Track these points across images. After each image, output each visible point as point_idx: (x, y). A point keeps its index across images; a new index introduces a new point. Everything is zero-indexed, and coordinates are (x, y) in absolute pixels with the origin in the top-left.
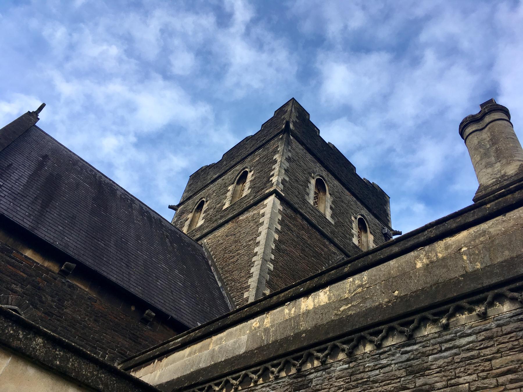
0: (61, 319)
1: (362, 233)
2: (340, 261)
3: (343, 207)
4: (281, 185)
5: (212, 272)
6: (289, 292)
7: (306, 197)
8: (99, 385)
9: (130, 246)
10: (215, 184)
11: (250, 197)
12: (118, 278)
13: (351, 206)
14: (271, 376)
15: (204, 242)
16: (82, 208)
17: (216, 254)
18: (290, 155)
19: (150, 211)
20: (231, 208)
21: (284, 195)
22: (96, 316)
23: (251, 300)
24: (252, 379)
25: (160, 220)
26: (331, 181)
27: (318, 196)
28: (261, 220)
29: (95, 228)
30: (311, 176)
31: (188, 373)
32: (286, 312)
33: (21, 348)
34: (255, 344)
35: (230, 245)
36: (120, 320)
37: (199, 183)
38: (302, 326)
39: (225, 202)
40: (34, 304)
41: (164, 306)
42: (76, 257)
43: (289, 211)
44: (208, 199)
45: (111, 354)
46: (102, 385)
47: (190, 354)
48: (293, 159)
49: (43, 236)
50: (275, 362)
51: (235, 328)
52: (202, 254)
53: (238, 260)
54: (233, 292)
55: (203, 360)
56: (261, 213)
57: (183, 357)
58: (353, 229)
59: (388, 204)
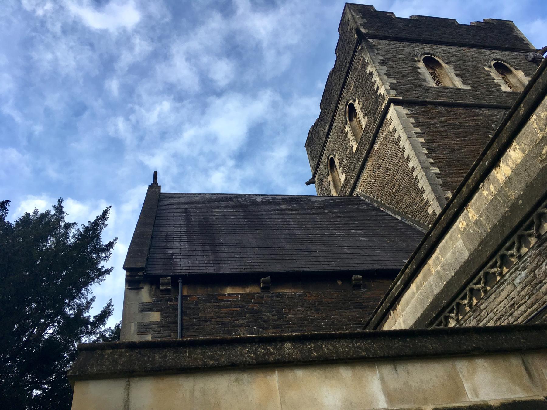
0: (290, 325)
1: (507, 76)
2: (503, 118)
3: (469, 66)
5: (384, 212)
6: (475, 174)
7: (425, 84)
8: (361, 353)
9: (300, 236)
10: (331, 137)
11: (370, 124)
12: (309, 266)
13: (477, 59)
14: (513, 259)
15: (358, 192)
16: (241, 231)
17: (376, 194)
19: (294, 198)
20: (360, 146)
21: (401, 98)
22: (315, 306)
23: (438, 211)
24: (494, 273)
25: (307, 199)
26: (439, 51)
27: (435, 74)
28: (396, 136)
29: (263, 240)
30: (416, 61)
31: (428, 304)
32: (485, 195)
33: (278, 359)
34: (475, 242)
35: (383, 178)
36: (335, 298)
37: (317, 146)
38: (512, 196)
39: (351, 145)
40: (262, 326)
41: (364, 265)
42: (265, 270)
43: (417, 109)
44: (334, 153)
45: (349, 329)
46: (364, 352)
47: (418, 289)
48: (386, 59)
49: (229, 270)
50: (508, 244)
51: (444, 241)
52: (364, 203)
53: (400, 185)
54: (415, 216)
55: (433, 287)
56: (391, 130)
57: (414, 295)
58: (495, 80)
59: (515, 29)
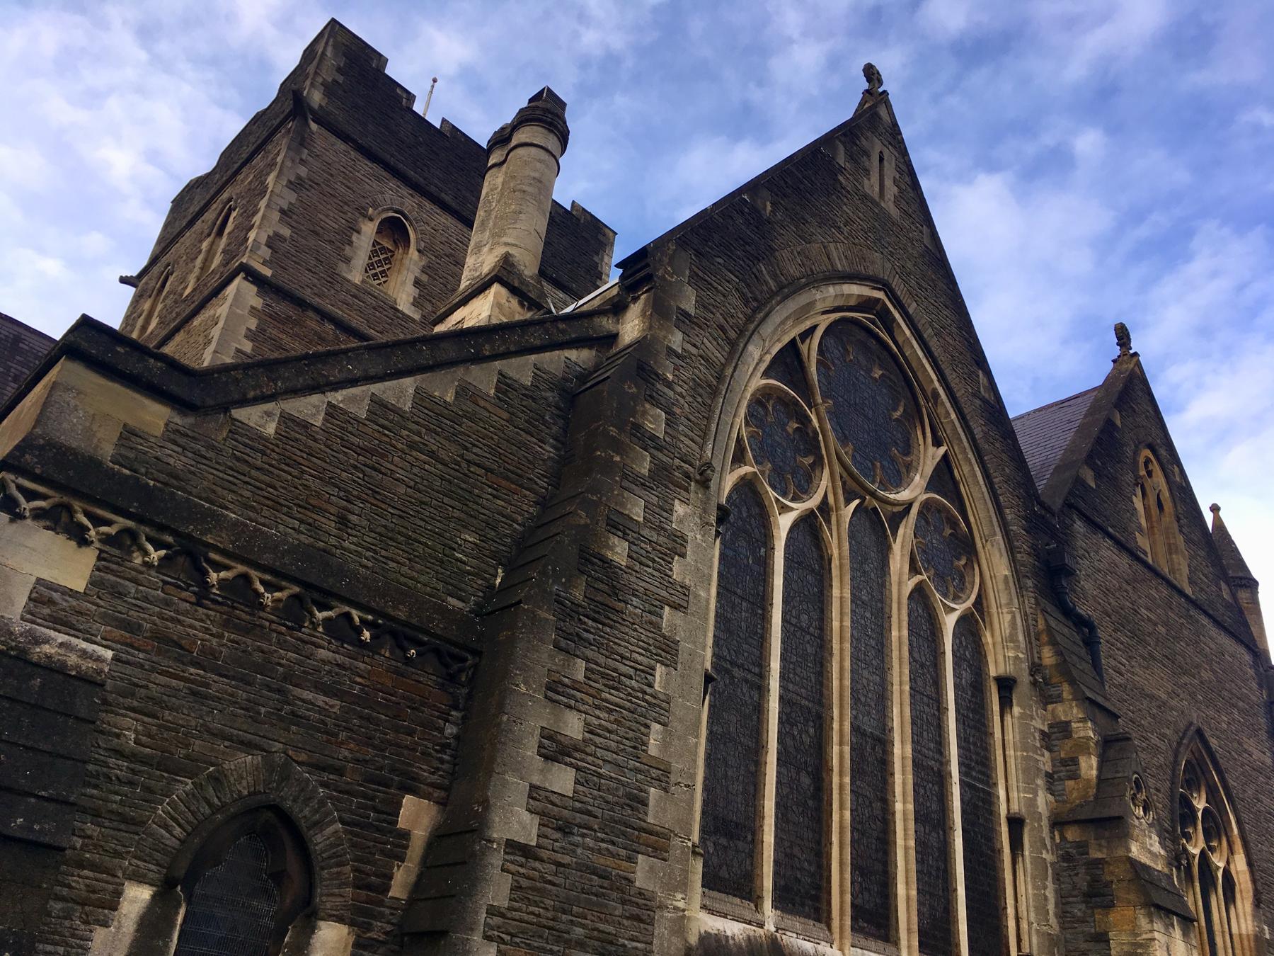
4: (266, 248)
18: (303, 171)
30: (365, 216)
43: (283, 308)
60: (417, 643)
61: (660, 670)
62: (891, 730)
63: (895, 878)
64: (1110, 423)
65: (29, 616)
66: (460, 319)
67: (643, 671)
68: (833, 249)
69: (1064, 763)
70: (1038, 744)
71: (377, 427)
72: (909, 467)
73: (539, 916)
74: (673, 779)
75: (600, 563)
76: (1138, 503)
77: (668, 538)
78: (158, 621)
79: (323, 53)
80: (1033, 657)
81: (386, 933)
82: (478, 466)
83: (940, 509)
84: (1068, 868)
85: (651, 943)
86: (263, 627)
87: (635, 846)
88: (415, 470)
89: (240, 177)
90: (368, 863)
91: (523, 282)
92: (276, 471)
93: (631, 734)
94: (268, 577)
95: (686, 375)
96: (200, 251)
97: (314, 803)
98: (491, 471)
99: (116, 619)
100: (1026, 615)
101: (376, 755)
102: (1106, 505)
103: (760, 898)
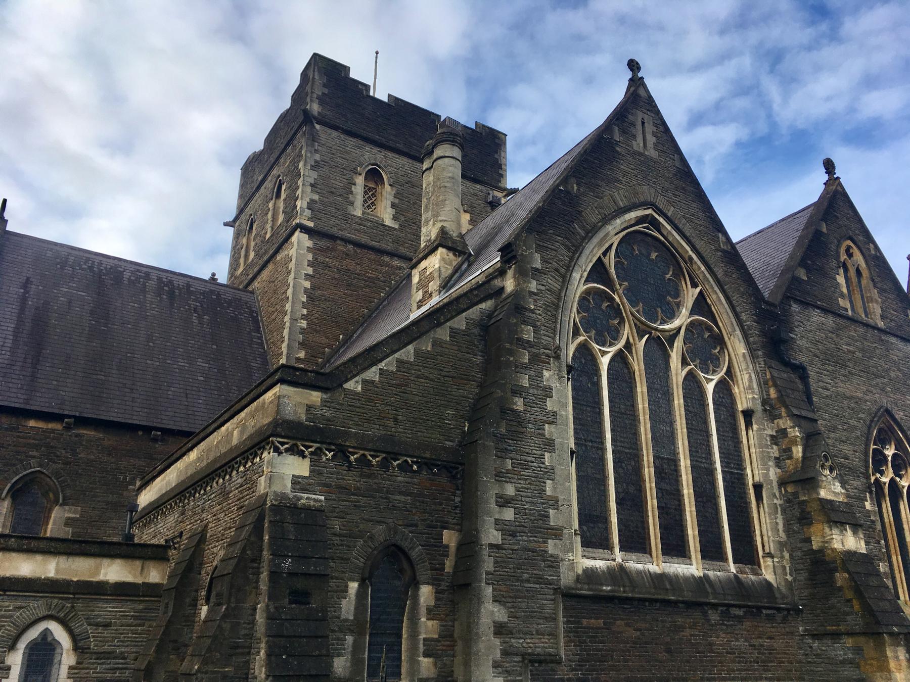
4: (308, 210)
18: (317, 157)
30: (356, 173)
43: (323, 243)
60: (437, 466)
61: (547, 455)
62: (678, 453)
63: (686, 527)
64: (818, 234)
65: (293, 490)
66: (424, 267)
67: (538, 458)
68: (617, 196)
69: (785, 451)
70: (769, 443)
71: (401, 373)
72: (678, 305)
73: (507, 572)
74: (560, 503)
75: (511, 412)
76: (841, 279)
77: (543, 390)
78: (337, 481)
79: (313, 78)
80: (763, 396)
81: (447, 586)
82: (448, 377)
83: (701, 323)
84: (789, 506)
85: (560, 576)
86: (374, 473)
87: (546, 536)
88: (421, 388)
89: (282, 160)
90: (434, 560)
91: (454, 242)
92: (365, 406)
93: (537, 488)
94: (372, 453)
95: (540, 303)
96: (269, 209)
97: (409, 540)
98: (454, 377)
99: (322, 483)
100: (757, 372)
101: (430, 516)
102: (815, 288)
103: (613, 547)
